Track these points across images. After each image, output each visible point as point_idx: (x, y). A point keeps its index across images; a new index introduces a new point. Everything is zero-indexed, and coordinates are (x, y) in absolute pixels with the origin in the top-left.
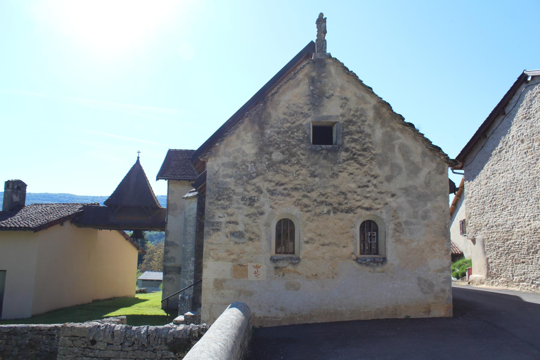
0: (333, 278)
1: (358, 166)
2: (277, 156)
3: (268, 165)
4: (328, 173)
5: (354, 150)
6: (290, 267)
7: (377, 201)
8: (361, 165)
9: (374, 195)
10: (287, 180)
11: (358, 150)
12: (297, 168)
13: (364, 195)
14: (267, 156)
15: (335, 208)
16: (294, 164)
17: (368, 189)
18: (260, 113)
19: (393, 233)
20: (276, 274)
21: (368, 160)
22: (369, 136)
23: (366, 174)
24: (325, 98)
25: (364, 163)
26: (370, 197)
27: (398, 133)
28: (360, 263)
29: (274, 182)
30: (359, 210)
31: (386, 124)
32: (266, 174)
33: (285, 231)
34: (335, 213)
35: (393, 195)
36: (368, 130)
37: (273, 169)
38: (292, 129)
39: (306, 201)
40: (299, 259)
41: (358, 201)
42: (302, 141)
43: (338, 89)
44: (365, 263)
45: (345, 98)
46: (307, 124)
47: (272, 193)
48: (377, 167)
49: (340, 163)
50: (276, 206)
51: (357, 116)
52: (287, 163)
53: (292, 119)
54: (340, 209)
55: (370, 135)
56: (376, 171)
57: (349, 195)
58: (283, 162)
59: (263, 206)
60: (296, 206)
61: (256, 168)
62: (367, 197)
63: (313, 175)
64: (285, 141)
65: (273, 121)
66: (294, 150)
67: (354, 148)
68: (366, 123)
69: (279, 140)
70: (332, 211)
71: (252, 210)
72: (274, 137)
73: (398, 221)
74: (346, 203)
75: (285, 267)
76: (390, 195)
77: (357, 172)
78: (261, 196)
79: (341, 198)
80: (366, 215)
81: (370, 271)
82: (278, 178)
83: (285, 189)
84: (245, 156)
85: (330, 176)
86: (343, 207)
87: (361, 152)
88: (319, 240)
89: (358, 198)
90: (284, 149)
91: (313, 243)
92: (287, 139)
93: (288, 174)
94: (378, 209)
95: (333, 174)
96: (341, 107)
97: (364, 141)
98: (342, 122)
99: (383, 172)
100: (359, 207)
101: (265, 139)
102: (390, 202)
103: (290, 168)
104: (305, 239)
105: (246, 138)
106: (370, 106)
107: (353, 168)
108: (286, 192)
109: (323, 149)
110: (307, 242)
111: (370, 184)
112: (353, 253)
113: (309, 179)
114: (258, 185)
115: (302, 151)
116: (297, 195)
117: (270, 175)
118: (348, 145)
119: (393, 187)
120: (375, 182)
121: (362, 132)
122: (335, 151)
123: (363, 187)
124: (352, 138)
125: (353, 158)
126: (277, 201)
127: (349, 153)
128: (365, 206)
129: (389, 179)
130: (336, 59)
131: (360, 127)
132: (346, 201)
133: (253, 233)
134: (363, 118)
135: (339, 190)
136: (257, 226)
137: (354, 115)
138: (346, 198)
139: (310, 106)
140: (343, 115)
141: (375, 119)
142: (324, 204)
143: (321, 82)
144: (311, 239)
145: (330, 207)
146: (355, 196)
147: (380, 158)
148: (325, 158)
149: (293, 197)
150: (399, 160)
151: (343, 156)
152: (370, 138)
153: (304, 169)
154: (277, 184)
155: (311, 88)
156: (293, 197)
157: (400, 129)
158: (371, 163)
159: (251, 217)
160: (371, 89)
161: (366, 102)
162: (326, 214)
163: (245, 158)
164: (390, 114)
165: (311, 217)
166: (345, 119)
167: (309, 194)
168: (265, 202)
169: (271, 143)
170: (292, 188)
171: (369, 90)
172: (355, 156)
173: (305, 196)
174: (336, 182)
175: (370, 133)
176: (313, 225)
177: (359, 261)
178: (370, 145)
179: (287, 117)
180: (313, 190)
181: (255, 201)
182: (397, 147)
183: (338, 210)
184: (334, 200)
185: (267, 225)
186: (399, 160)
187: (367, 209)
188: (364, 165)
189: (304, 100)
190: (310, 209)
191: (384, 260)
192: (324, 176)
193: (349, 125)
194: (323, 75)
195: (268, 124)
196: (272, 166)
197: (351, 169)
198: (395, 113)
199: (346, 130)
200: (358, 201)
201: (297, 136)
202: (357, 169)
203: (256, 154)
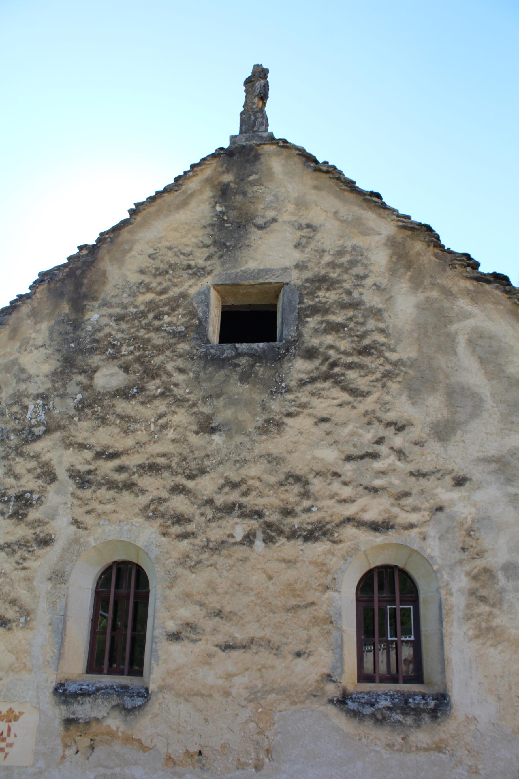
0: (258, 768)
1: (345, 397)
2: (108, 377)
3: (81, 401)
4: (252, 421)
5: (331, 352)
6: (114, 722)
7: (408, 501)
8: (355, 392)
9: (396, 481)
10: (129, 442)
11: (346, 353)
12: (163, 408)
13: (365, 483)
14: (81, 378)
15: (269, 525)
16: (155, 397)
17: (378, 465)
18: (78, 272)
19: (468, 606)
20: (66, 746)
21: (377, 380)
22: (377, 313)
23: (370, 419)
24: (254, 229)
25: (364, 388)
26: (384, 489)
27: (463, 303)
28: (355, 714)
29: (90, 448)
30: (350, 531)
31: (426, 282)
32: (72, 427)
33: (122, 597)
34: (269, 540)
35: (460, 482)
36: (371, 299)
37: (94, 413)
38: (158, 307)
39: (179, 504)
40: (145, 694)
41: (345, 501)
42: (181, 336)
43: (291, 207)
44: (373, 715)
45: (309, 226)
46: (199, 293)
47: (82, 480)
48: (404, 398)
49: (289, 390)
50: (89, 520)
51: (341, 265)
52: (134, 396)
53: (160, 284)
54: (286, 529)
55: (379, 310)
56: (402, 408)
57: (317, 485)
58: (123, 393)
59: (53, 517)
60: (148, 518)
61: (48, 412)
62: (375, 490)
63: (207, 427)
64: (135, 338)
65: (109, 291)
66: (158, 360)
67: (331, 347)
68: (369, 282)
69: (119, 336)
70: (260, 535)
71: (21, 532)
72: (107, 330)
73: (480, 563)
74: (308, 510)
75: (97, 720)
76: (448, 480)
77: (344, 412)
78: (51, 489)
79: (291, 495)
80: (368, 551)
81: (390, 746)
82: (106, 437)
83: (121, 469)
84: (25, 381)
85: (258, 428)
86: (296, 522)
87: (356, 359)
88: (215, 631)
89: (347, 492)
90: (131, 357)
91: (195, 641)
92: (142, 333)
93: (133, 426)
94: (412, 526)
95: (268, 421)
96: (297, 246)
97: (363, 329)
98: (299, 283)
99: (424, 412)
100: (349, 520)
101: (83, 334)
102: (452, 503)
103: (141, 408)
104: (171, 626)
105: (33, 335)
106: (381, 239)
107: (329, 402)
108: (122, 477)
109: (239, 355)
110: (175, 637)
111: (383, 449)
112: (329, 678)
113: (193, 439)
114: (44, 458)
115: (180, 363)
116: (153, 485)
117: (83, 430)
118: (315, 342)
119: (459, 454)
120: (398, 441)
121: (355, 305)
122: (277, 358)
123: (362, 457)
124: (328, 322)
125: (330, 374)
126: (94, 505)
127: (317, 362)
128: (368, 517)
129: (443, 431)
130: (285, 141)
131: (349, 293)
132: (306, 503)
133: (13, 602)
134: (359, 270)
135: (285, 469)
136: (28, 579)
137: (332, 265)
138: (305, 495)
139: (212, 249)
140: (300, 267)
141: (393, 272)
142: (236, 512)
143: (244, 193)
144: (190, 626)
145: (254, 524)
146: (336, 486)
147: (411, 372)
148: (244, 378)
149: (143, 491)
150: (471, 373)
151: (299, 371)
152: (380, 320)
153: (183, 411)
154: (99, 455)
155: (218, 208)
156: (143, 491)
157: (467, 292)
158: (384, 386)
159: (14, 552)
160: (378, 195)
161: (366, 232)
162: (241, 543)
163: (23, 387)
164: (436, 255)
165: (193, 556)
166: (308, 274)
167: (190, 484)
168: (58, 506)
169: (97, 346)
170: (141, 466)
171: (373, 200)
172: (336, 370)
173: (178, 489)
174: (274, 445)
175: (380, 306)
176: (196, 581)
177: (351, 705)
178: (382, 339)
179: (147, 279)
180: (203, 471)
181: (31, 505)
182: (462, 340)
183: (281, 532)
184: (269, 501)
185: (58, 577)
186: (471, 373)
187: (375, 527)
188: (365, 395)
189: (197, 237)
190: (190, 527)
191: (440, 705)
192: (241, 430)
193: (319, 288)
194: (251, 178)
195: (95, 299)
196: (90, 406)
197: (321, 406)
198: (449, 252)
199: (308, 302)
200: (345, 501)
201: (169, 324)
202: (340, 405)
203: (55, 373)
